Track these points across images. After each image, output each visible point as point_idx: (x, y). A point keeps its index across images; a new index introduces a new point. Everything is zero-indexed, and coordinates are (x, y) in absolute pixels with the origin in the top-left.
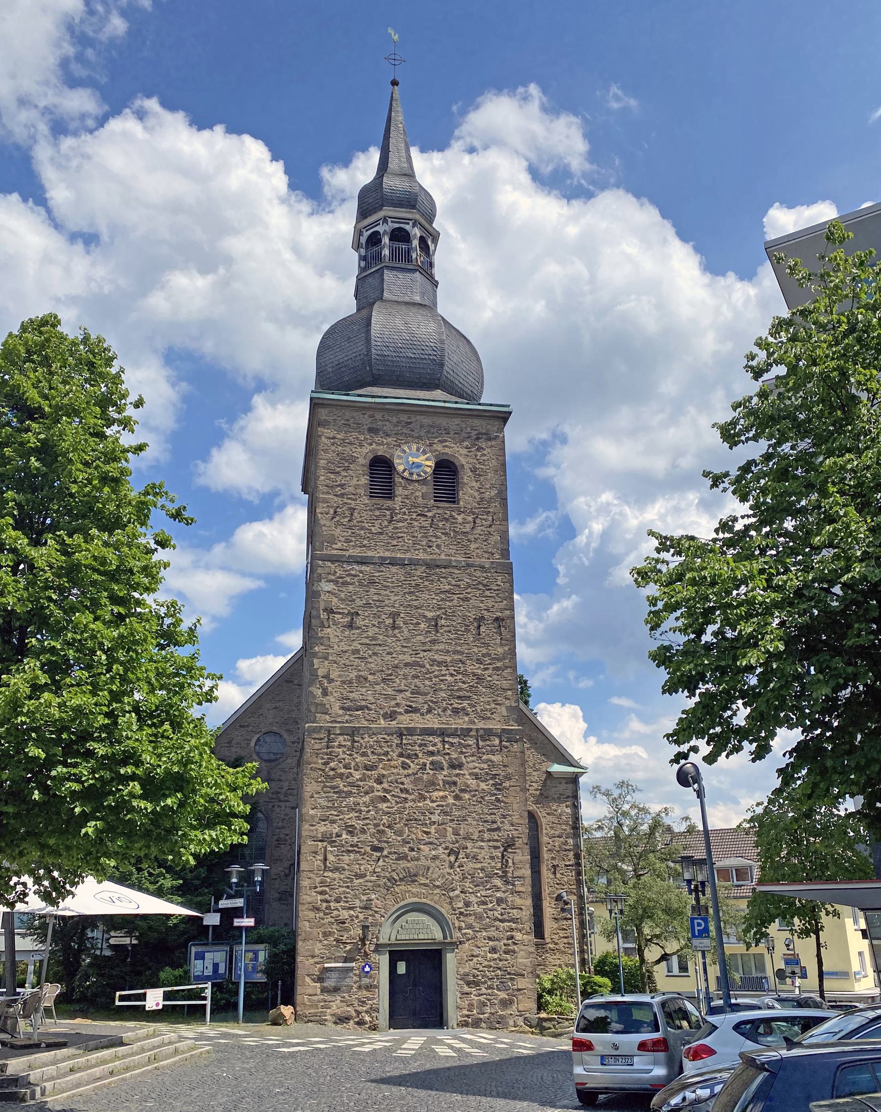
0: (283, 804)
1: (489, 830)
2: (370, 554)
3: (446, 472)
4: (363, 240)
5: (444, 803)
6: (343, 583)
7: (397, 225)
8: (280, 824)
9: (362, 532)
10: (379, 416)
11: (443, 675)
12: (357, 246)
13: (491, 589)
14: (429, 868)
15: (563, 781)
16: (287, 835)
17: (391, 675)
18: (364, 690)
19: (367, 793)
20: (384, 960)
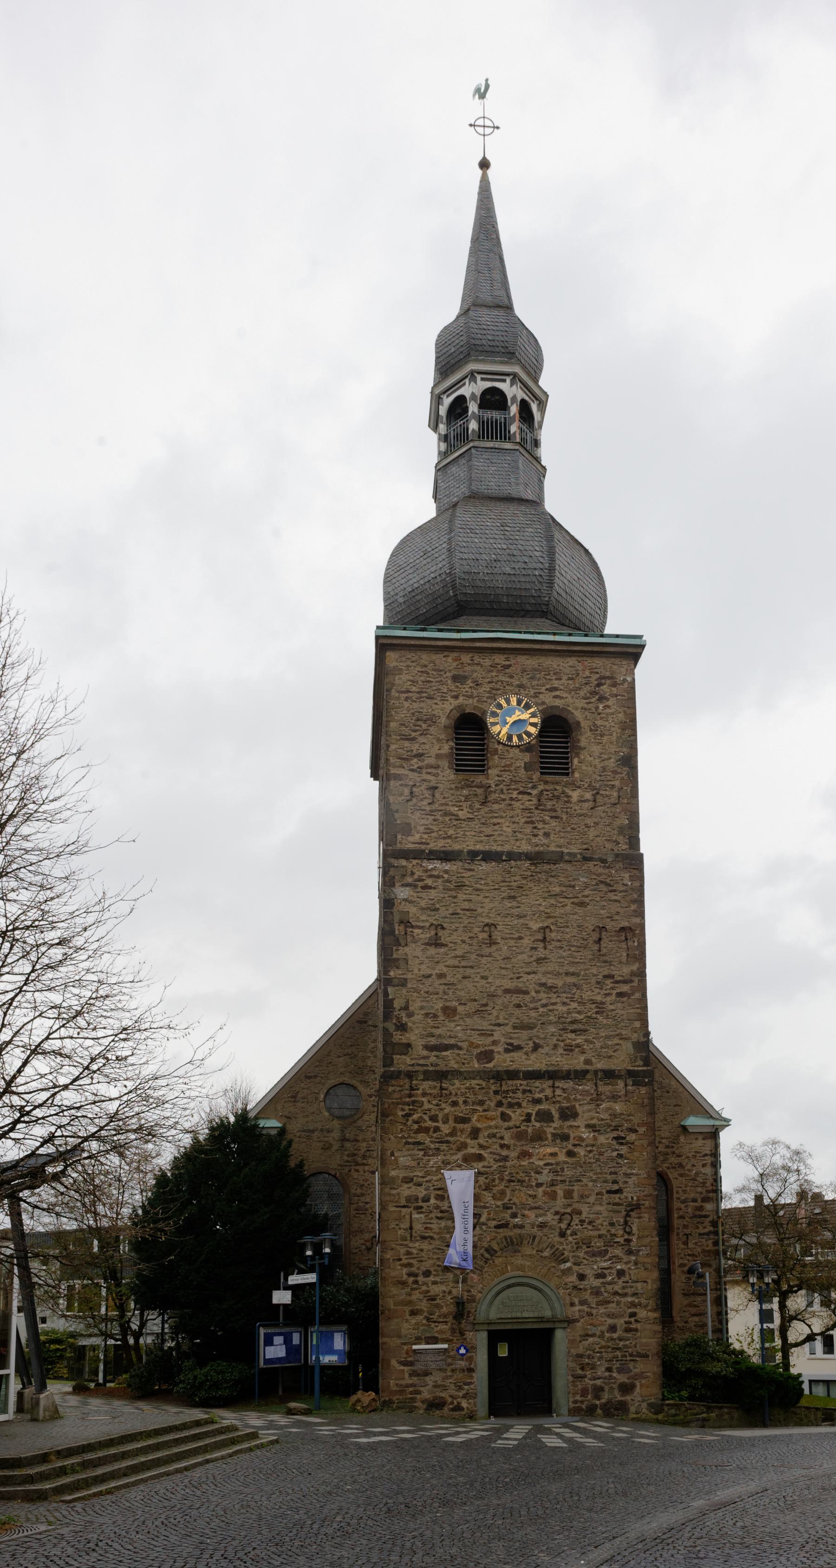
0: (360, 1168)
1: (609, 1192)
2: (457, 847)
3: (557, 730)
4: (443, 411)
5: (553, 1161)
6: (422, 888)
7: (489, 384)
8: (359, 1191)
9: (447, 819)
10: (466, 658)
11: (553, 1004)
12: (434, 425)
13: (615, 891)
14: (534, 1237)
15: (700, 1137)
16: (367, 1203)
17: (486, 1005)
18: (452, 1025)
19: (459, 1150)
20: (481, 1340)
